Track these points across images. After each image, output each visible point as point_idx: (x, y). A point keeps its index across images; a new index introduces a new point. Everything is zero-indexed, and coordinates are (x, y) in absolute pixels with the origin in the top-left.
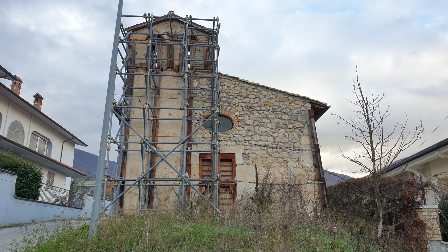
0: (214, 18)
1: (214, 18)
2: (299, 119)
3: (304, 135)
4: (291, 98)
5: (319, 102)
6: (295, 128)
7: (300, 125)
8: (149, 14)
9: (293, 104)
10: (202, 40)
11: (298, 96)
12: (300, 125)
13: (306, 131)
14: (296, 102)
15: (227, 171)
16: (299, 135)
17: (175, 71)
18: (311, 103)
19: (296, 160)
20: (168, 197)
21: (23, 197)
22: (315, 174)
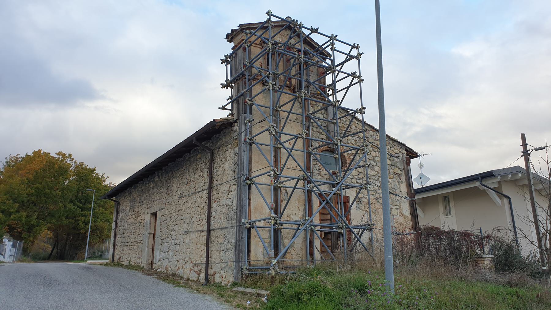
0: (354, 44)
1: (354, 44)
2: (399, 165)
3: (402, 182)
4: (391, 142)
5: (412, 150)
6: (395, 174)
7: (399, 172)
8: (297, 21)
9: (393, 149)
10: (228, 35)
11: (404, 145)
12: (399, 172)
13: (403, 178)
14: (395, 147)
15: (545, 245)
16: (399, 182)
17: (291, 91)
18: (406, 150)
19: (398, 207)
20: (295, 252)
21: (62, 259)
22: (411, 223)
